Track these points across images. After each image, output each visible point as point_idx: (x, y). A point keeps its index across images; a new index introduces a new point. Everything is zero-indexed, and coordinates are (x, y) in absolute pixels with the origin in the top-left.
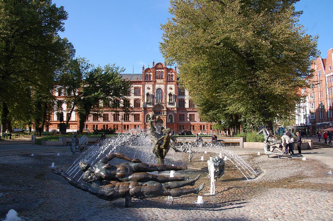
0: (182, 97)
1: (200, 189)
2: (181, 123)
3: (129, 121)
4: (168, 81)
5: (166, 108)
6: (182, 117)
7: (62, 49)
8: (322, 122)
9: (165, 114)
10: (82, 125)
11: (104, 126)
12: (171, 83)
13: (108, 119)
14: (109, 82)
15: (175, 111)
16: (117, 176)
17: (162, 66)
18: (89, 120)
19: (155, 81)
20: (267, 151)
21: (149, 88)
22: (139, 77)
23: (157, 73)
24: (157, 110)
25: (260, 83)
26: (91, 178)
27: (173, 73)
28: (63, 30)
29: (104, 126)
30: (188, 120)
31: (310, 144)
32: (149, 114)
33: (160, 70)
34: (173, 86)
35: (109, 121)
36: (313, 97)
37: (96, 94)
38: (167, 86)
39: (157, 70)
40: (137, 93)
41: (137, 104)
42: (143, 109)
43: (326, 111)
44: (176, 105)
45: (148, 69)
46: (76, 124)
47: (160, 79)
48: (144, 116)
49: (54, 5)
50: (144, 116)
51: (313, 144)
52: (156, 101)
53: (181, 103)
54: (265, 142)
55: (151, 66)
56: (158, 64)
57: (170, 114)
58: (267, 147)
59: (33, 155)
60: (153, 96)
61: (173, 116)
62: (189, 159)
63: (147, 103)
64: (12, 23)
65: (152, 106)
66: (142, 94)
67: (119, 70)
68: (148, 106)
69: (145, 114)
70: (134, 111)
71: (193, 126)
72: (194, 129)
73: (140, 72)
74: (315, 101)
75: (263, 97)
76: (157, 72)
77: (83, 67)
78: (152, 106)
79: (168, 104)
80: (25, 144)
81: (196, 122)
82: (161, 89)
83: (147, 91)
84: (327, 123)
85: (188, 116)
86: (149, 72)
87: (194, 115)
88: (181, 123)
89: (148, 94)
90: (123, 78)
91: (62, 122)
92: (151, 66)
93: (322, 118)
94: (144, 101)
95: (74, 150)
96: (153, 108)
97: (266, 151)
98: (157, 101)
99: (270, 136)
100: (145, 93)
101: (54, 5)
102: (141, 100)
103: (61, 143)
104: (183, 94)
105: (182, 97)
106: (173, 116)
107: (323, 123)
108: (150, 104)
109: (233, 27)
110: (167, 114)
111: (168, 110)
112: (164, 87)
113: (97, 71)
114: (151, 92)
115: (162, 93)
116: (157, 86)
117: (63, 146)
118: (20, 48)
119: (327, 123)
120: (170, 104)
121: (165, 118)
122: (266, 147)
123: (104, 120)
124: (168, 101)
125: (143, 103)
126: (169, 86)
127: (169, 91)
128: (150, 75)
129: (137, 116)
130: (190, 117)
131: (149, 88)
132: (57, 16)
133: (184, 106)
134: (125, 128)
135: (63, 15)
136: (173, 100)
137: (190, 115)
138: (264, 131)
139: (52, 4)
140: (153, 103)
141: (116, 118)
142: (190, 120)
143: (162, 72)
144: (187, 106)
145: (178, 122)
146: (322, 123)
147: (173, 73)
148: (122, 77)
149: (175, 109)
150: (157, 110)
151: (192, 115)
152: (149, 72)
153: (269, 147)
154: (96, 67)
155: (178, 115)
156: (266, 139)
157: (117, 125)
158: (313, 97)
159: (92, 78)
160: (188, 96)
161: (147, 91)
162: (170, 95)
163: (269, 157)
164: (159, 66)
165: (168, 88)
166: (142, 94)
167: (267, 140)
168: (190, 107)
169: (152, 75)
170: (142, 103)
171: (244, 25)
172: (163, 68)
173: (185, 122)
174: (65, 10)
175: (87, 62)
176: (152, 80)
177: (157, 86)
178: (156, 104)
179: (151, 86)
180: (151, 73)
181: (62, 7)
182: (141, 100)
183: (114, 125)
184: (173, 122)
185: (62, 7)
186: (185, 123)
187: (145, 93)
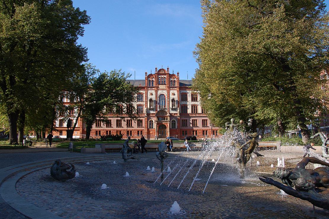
0: (183, 103)
2: (185, 128)
3: (207, 127)
4: (171, 86)
5: (170, 114)
6: (185, 123)
7: (80, 54)
9: (169, 119)
10: (87, 131)
11: (107, 131)
12: (173, 89)
13: (121, 125)
14: (118, 87)
15: (178, 116)
16: (321, 182)
17: (165, 72)
18: (112, 126)
19: (158, 87)
21: (174, 94)
22: (141, 82)
23: (159, 79)
24: (161, 115)
25: (299, 88)
26: (309, 186)
27: (175, 79)
28: (82, 35)
29: (107, 131)
30: (191, 125)
32: (153, 120)
33: (162, 76)
34: (176, 92)
35: (133, 127)
37: (106, 99)
38: (147, 92)
39: (160, 76)
40: (140, 98)
41: (140, 111)
42: (146, 114)
44: (178, 111)
45: (151, 75)
46: (79, 130)
47: (162, 85)
48: (147, 122)
49: (78, 9)
50: (147, 122)
52: (158, 107)
53: (184, 108)
54: (323, 145)
55: (154, 72)
56: (160, 70)
57: (174, 119)
58: (325, 150)
59: (88, 163)
60: (156, 102)
61: (176, 122)
63: (150, 109)
64: (41, 25)
65: (155, 112)
66: (144, 100)
67: (125, 76)
68: (152, 112)
69: (148, 120)
70: (140, 117)
71: (196, 131)
72: (196, 134)
73: (143, 78)
75: (299, 102)
76: (160, 78)
77: (89, 73)
78: (155, 112)
79: (171, 109)
80: (53, 152)
81: (198, 127)
82: (163, 94)
83: (150, 97)
85: (191, 122)
86: (152, 78)
87: (197, 120)
88: (185, 128)
89: (151, 100)
90: (131, 84)
91: (70, 129)
92: (154, 72)
94: (147, 107)
95: (127, 157)
96: (157, 114)
98: (160, 107)
100: (171, 99)
101: (78, 9)
102: (144, 106)
103: (100, 150)
104: (186, 100)
105: (183, 103)
106: (176, 122)
108: (153, 109)
109: (273, 32)
110: (170, 119)
111: (171, 116)
112: (166, 93)
113: (103, 76)
114: (154, 97)
115: (165, 99)
116: (160, 92)
117: (102, 153)
120: (173, 109)
121: (169, 124)
122: (324, 150)
123: (107, 127)
124: (171, 107)
125: (146, 109)
126: (171, 92)
127: (172, 97)
128: (152, 81)
129: (195, 121)
130: (193, 123)
131: (152, 94)
132: (79, 19)
133: (187, 111)
134: (203, 134)
135: (85, 19)
136: (176, 106)
137: (193, 120)
139: (75, 9)
140: (156, 108)
141: (119, 124)
142: (193, 125)
143: (165, 78)
144: (189, 111)
145: (181, 128)
147: (175, 79)
148: (130, 82)
149: (178, 114)
150: (161, 115)
151: (195, 120)
152: (152, 78)
154: (102, 72)
155: (181, 121)
156: (325, 142)
157: (120, 131)
159: (100, 83)
160: (188, 103)
161: (150, 97)
162: (173, 100)
164: (162, 72)
165: (171, 93)
166: (144, 100)
167: (326, 143)
168: (192, 112)
169: (155, 81)
170: (145, 109)
171: (290, 30)
172: (165, 74)
173: (187, 127)
174: (87, 14)
175: (93, 68)
176: (154, 85)
177: (160, 92)
178: (159, 110)
179: (153, 92)
180: (154, 79)
181: (85, 11)
182: (144, 106)
183: (117, 131)
184: (176, 127)
185: (85, 11)
186: (188, 128)
187: (171, 99)
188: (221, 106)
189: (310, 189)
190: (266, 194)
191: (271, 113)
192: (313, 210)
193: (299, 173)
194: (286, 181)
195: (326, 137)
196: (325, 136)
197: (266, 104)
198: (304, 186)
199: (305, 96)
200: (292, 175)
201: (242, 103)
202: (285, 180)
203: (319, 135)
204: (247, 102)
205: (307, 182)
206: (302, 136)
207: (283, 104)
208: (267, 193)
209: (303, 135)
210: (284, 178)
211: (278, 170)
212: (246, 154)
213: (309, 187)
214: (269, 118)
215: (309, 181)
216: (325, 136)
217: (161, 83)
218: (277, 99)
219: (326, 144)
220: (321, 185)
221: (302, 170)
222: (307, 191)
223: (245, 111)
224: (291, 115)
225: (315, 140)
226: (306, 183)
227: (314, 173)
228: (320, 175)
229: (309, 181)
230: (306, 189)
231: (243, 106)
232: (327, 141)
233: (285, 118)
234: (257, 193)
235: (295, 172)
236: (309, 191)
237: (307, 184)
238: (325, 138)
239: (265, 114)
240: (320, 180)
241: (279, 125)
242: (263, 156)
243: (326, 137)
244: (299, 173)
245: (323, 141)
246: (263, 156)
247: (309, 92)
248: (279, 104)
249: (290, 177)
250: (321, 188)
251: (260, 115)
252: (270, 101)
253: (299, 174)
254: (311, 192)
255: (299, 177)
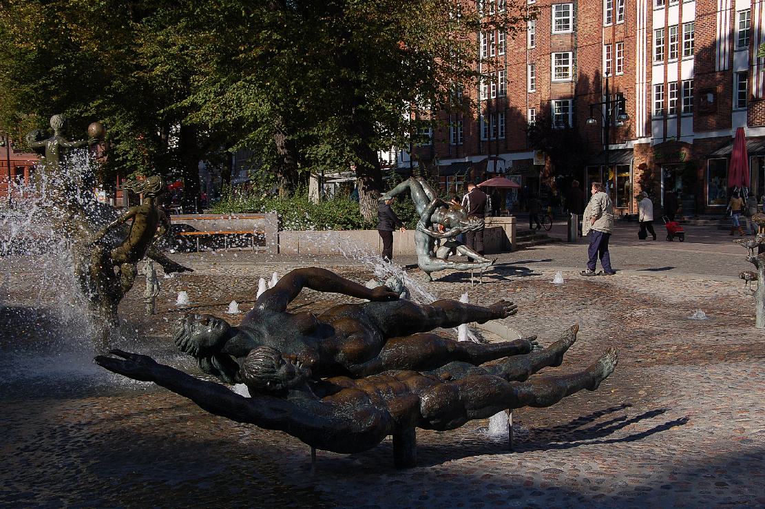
1: (605, 375)
8: (457, 157)
20: (427, 259)
26: (291, 373)
31: (509, 233)
36: (571, 24)
43: (475, 116)
51: (516, 233)
58: (427, 245)
62: (148, 301)
74: (581, 41)
75: (352, 61)
84: (477, 159)
93: (456, 141)
97: (424, 260)
99: (437, 205)
107: (462, 161)
118: (81, 113)
119: (477, 159)
122: (422, 244)
138: (414, 187)
146: (458, 161)
153: (431, 243)
156: (425, 216)
158: (571, 24)
163: (431, 280)
188: (45, 60)
189: (294, 387)
190: (174, 421)
191: (250, 101)
192: (310, 462)
193: (264, 329)
194: (214, 361)
195: (431, 197)
196: (427, 191)
197: (230, 65)
198: (269, 377)
199: (376, 36)
200: (234, 339)
201: (136, 55)
202: (209, 361)
203: (408, 189)
204: (158, 48)
205: (284, 362)
206: (361, 193)
207: (291, 65)
208: (179, 414)
209: (363, 189)
210: (204, 351)
211: (184, 322)
212: (119, 263)
213: (290, 379)
214: (241, 120)
215: (291, 359)
216: (427, 191)
217: (713, 69)
218: (271, 46)
219: (429, 224)
220: (340, 370)
221: (275, 319)
222: (284, 393)
223: (149, 89)
224: (321, 112)
225: (403, 209)
226: (279, 366)
227: (317, 329)
228: (337, 332)
229: (291, 359)
230: (279, 386)
231: (139, 67)
232: (432, 212)
233: (294, 121)
234: (139, 420)
235: (247, 328)
236: (289, 393)
237: (282, 370)
238: (428, 201)
239: (225, 104)
240: (336, 351)
241: (282, 152)
242: (188, 270)
243: (431, 197)
244: (264, 329)
245: (422, 209)
246: (188, 270)
247: (388, 23)
248: (277, 64)
249: (227, 347)
250: (336, 381)
251: (210, 103)
252: (245, 51)
253: (260, 335)
254: (297, 397)
255: (257, 346)
